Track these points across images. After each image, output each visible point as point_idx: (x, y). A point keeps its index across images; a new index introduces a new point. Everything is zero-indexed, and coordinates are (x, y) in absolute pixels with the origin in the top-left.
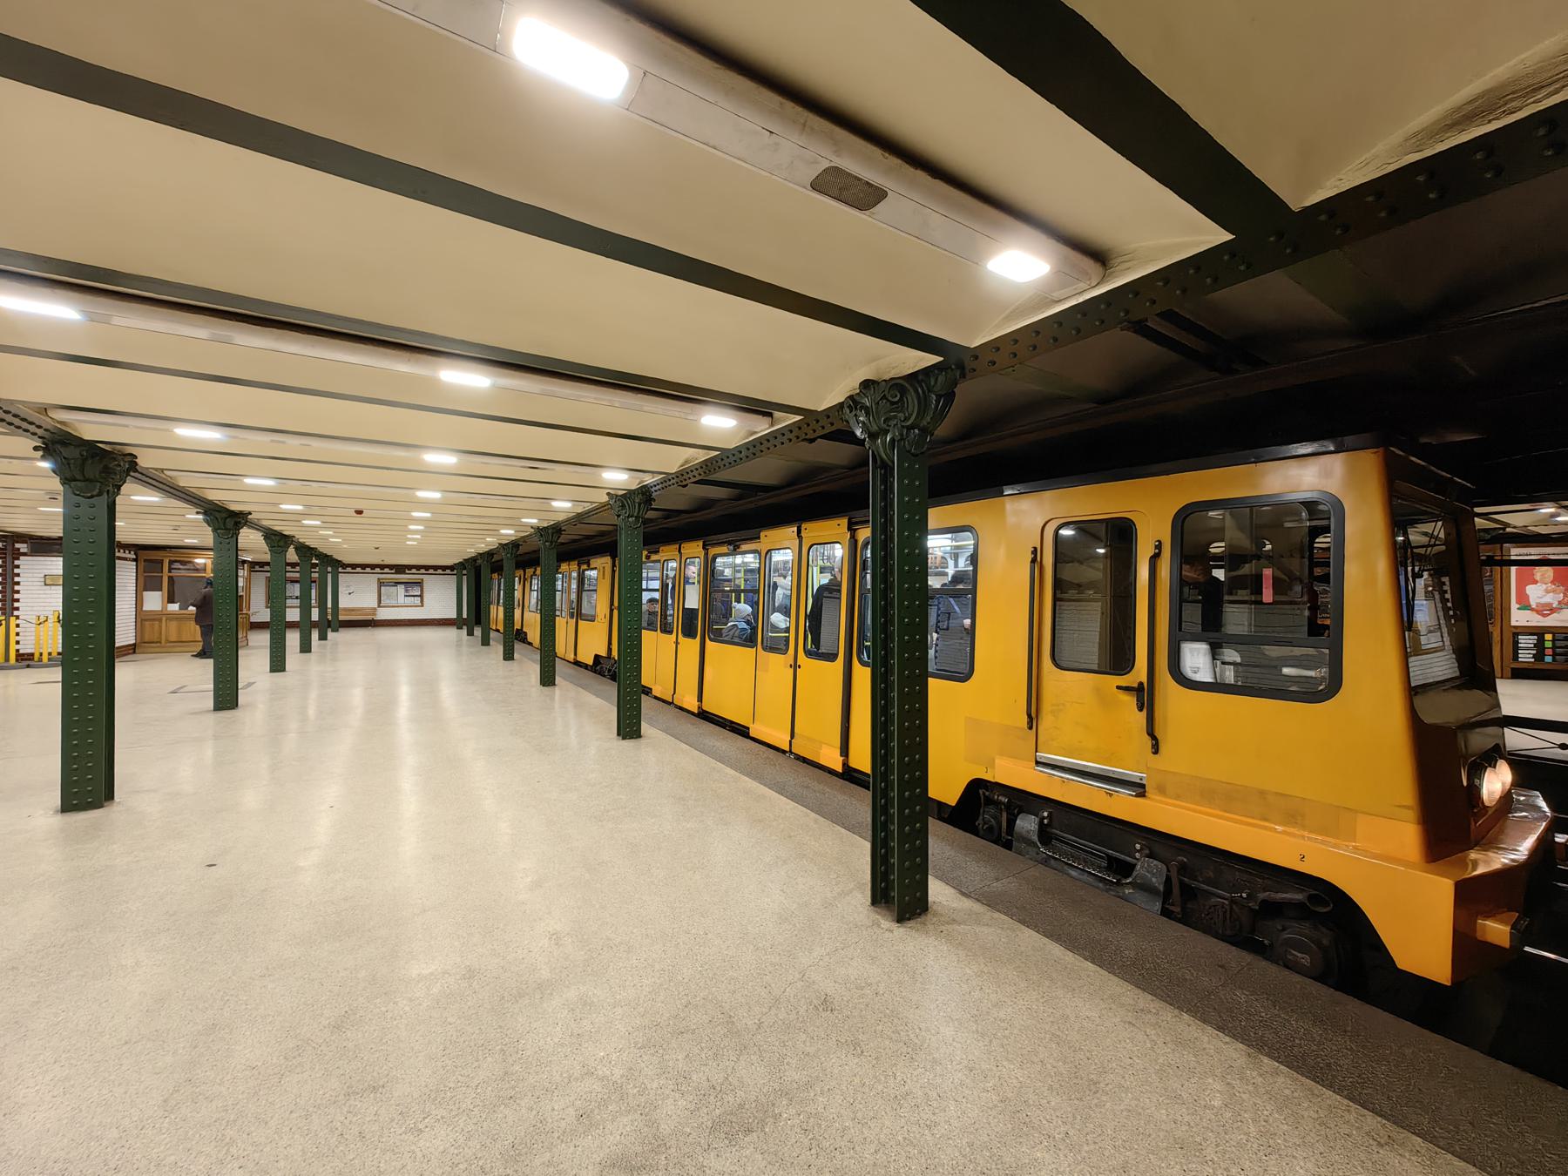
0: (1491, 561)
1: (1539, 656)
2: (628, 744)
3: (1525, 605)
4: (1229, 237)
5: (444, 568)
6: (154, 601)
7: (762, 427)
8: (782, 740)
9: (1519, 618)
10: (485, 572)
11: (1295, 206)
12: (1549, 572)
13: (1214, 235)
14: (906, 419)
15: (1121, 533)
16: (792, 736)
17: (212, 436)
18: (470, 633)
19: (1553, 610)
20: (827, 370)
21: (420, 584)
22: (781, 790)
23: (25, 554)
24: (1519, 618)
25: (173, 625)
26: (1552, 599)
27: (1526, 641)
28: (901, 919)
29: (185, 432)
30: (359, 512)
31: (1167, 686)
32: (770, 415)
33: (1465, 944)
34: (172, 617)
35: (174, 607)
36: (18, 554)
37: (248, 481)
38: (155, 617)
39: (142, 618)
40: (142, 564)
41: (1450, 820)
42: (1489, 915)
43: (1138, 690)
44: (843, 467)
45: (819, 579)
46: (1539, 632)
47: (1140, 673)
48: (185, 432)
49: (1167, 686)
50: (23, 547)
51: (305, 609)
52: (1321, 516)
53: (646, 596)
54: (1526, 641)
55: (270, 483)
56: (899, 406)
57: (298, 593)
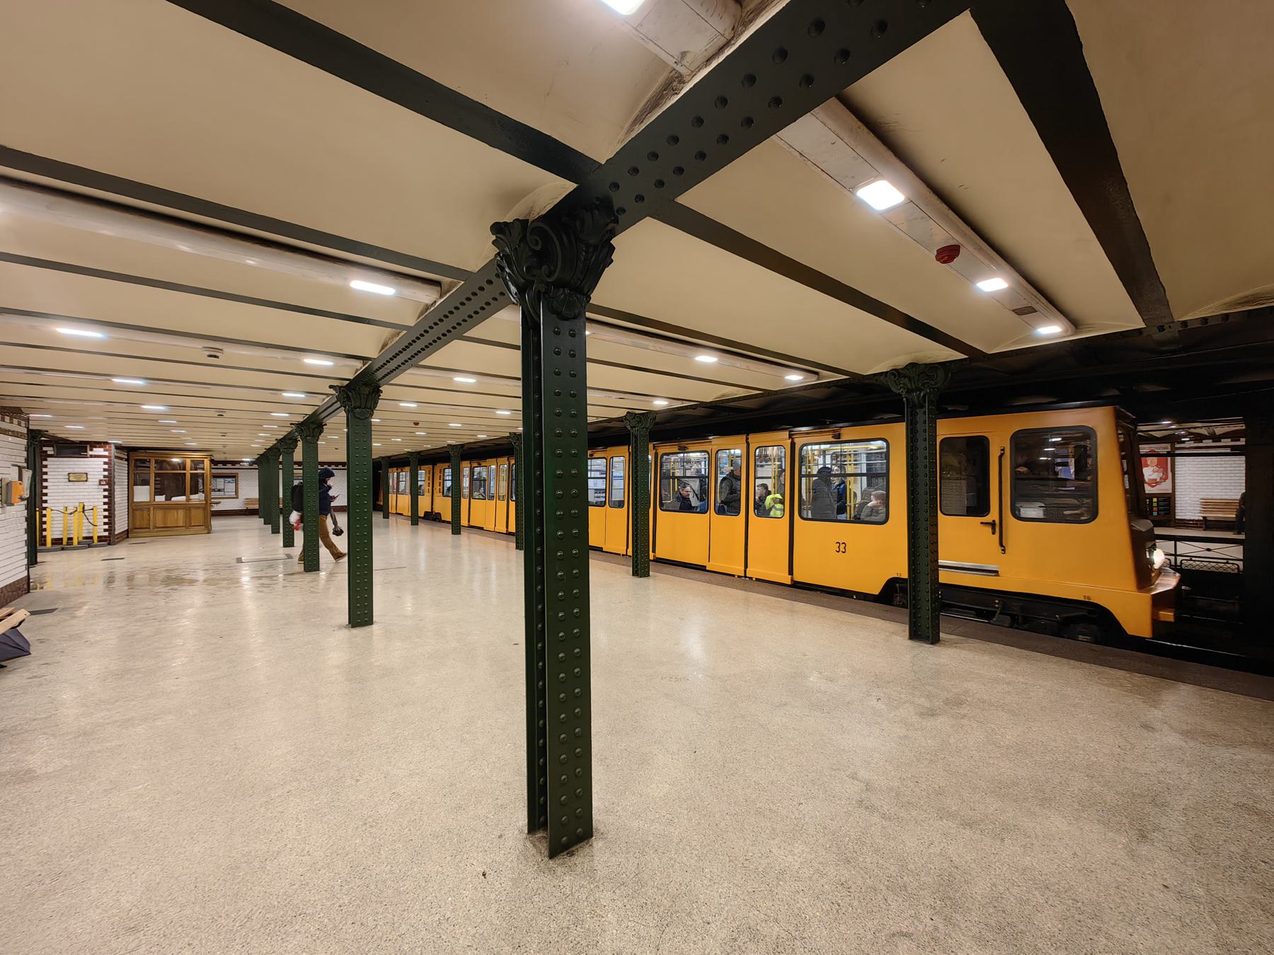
6: (143, 494)
7: (813, 380)
8: (738, 569)
12: (1155, 459)
14: (550, 274)
15: (977, 448)
16: (746, 566)
17: (94, 334)
19: (1157, 483)
20: (876, 348)
21: (234, 476)
22: (776, 596)
23: (51, 456)
25: (160, 514)
28: (932, 643)
29: (67, 331)
30: (416, 424)
31: (1010, 520)
32: (816, 373)
33: (1156, 622)
34: (160, 506)
36: (46, 456)
37: (116, 380)
39: (133, 507)
40: (132, 463)
41: (1144, 574)
42: (1164, 609)
43: (993, 524)
44: (820, 400)
45: (727, 468)
47: (993, 515)
48: (67, 331)
49: (1010, 520)
50: (50, 450)
51: (1151, 502)
52: (1087, 434)
53: (591, 483)
55: (140, 382)
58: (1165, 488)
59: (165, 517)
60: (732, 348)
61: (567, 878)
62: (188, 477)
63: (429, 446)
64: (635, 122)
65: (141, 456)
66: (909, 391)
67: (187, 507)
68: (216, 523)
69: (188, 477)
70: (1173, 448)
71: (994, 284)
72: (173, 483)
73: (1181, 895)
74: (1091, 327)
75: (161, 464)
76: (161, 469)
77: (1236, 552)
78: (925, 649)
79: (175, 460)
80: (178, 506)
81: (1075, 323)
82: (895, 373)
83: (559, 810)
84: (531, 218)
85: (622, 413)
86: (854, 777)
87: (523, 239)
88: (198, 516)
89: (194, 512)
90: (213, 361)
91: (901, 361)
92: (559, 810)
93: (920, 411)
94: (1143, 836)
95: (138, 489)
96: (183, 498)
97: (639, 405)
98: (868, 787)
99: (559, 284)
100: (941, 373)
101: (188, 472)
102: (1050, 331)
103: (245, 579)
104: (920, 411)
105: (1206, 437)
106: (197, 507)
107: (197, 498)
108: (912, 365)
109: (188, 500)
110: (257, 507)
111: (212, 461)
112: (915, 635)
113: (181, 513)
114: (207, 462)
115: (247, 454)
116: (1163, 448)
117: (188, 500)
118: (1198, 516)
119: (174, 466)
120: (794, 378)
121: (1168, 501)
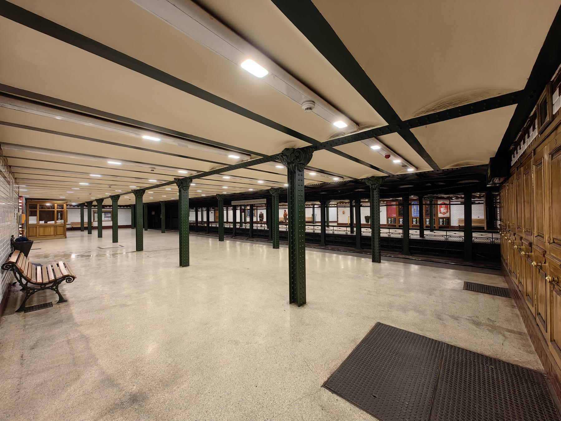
0: (351, 203)
1: (443, 224)
2: (295, 308)
3: (441, 213)
4: (515, 106)
5: (127, 206)
7: (341, 180)
9: (440, 215)
10: (275, 200)
11: (396, 134)
13: (412, 130)
14: (300, 161)
18: (90, 233)
24: (440, 215)
25: (42, 229)
26: (445, 211)
27: (441, 220)
29: (111, 163)
34: (41, 226)
35: (42, 222)
38: (34, 226)
46: (443, 218)
54: (441, 220)
56: (297, 157)
57: (382, 230)
58: (447, 215)
59: (44, 231)
60: (321, 171)
61: (303, 311)
62: (56, 212)
63: (173, 199)
64: (332, 137)
65: (33, 203)
66: (372, 185)
67: (55, 227)
68: (68, 234)
69: (56, 212)
70: (450, 202)
71: (397, 161)
72: (47, 215)
73: (436, 302)
74: (421, 169)
75: (42, 207)
76: (42, 208)
77: (462, 234)
78: (377, 264)
79: (48, 204)
80: (51, 226)
81: (417, 168)
82: (368, 179)
83: (297, 296)
84: (296, 147)
85: (269, 188)
86: (365, 290)
87: (293, 153)
88: (60, 230)
89: (58, 228)
90: (152, 172)
91: (369, 175)
92: (297, 296)
93: (375, 191)
94: (430, 295)
95: (30, 218)
96: (53, 222)
97: (276, 186)
98: (369, 291)
99: (300, 164)
100: (381, 180)
101: (56, 210)
102: (411, 170)
103: (108, 255)
104: (375, 191)
105: (459, 198)
106: (60, 226)
107: (60, 222)
108: (373, 177)
109: (56, 223)
110: (80, 226)
111: (67, 205)
112: (374, 261)
113: (52, 229)
114: (65, 205)
115: (75, 201)
116: (447, 202)
117: (56, 223)
118: (457, 225)
119: (48, 208)
120: (336, 179)
121: (448, 220)
